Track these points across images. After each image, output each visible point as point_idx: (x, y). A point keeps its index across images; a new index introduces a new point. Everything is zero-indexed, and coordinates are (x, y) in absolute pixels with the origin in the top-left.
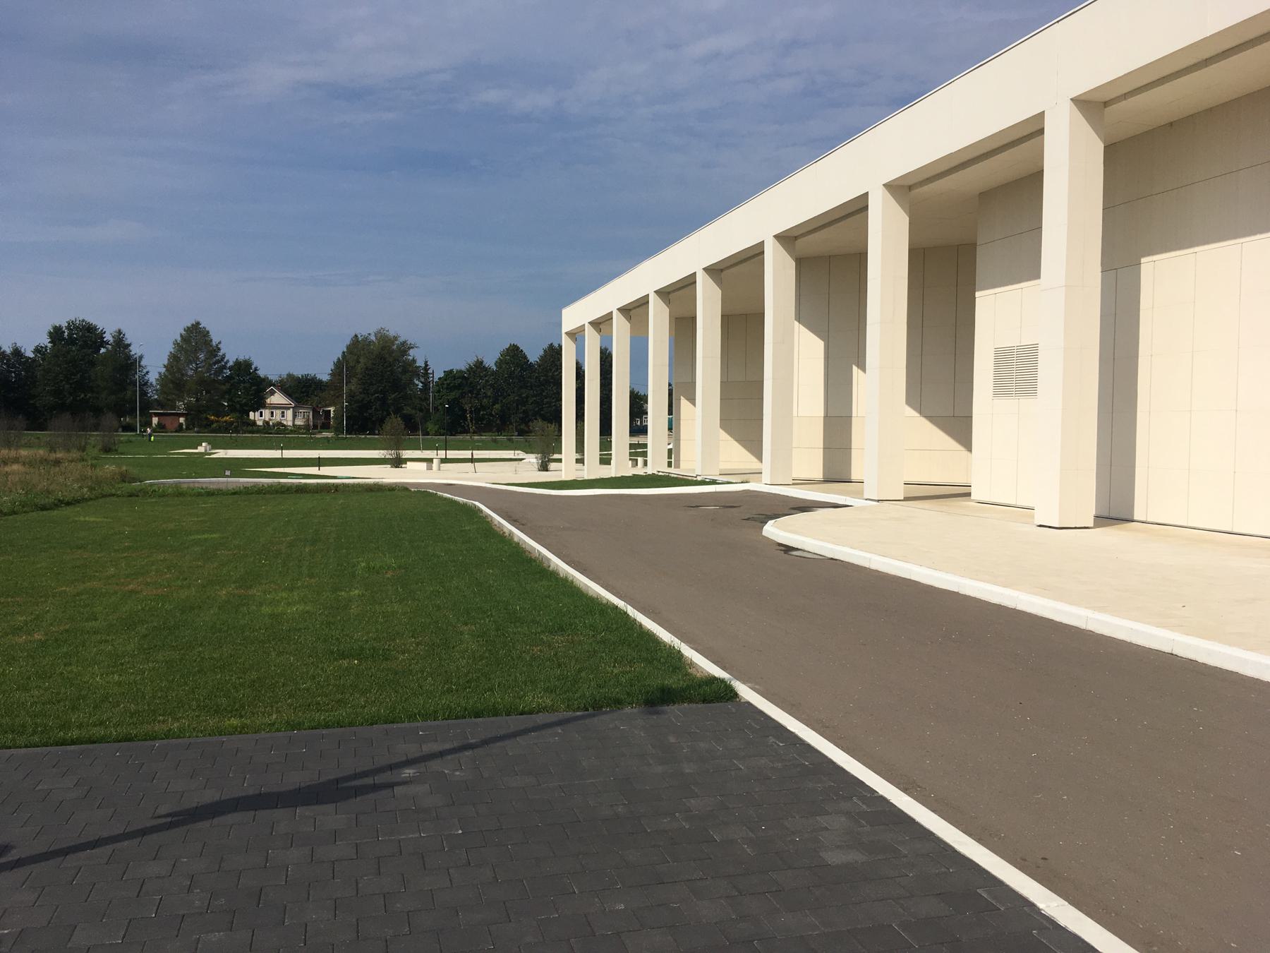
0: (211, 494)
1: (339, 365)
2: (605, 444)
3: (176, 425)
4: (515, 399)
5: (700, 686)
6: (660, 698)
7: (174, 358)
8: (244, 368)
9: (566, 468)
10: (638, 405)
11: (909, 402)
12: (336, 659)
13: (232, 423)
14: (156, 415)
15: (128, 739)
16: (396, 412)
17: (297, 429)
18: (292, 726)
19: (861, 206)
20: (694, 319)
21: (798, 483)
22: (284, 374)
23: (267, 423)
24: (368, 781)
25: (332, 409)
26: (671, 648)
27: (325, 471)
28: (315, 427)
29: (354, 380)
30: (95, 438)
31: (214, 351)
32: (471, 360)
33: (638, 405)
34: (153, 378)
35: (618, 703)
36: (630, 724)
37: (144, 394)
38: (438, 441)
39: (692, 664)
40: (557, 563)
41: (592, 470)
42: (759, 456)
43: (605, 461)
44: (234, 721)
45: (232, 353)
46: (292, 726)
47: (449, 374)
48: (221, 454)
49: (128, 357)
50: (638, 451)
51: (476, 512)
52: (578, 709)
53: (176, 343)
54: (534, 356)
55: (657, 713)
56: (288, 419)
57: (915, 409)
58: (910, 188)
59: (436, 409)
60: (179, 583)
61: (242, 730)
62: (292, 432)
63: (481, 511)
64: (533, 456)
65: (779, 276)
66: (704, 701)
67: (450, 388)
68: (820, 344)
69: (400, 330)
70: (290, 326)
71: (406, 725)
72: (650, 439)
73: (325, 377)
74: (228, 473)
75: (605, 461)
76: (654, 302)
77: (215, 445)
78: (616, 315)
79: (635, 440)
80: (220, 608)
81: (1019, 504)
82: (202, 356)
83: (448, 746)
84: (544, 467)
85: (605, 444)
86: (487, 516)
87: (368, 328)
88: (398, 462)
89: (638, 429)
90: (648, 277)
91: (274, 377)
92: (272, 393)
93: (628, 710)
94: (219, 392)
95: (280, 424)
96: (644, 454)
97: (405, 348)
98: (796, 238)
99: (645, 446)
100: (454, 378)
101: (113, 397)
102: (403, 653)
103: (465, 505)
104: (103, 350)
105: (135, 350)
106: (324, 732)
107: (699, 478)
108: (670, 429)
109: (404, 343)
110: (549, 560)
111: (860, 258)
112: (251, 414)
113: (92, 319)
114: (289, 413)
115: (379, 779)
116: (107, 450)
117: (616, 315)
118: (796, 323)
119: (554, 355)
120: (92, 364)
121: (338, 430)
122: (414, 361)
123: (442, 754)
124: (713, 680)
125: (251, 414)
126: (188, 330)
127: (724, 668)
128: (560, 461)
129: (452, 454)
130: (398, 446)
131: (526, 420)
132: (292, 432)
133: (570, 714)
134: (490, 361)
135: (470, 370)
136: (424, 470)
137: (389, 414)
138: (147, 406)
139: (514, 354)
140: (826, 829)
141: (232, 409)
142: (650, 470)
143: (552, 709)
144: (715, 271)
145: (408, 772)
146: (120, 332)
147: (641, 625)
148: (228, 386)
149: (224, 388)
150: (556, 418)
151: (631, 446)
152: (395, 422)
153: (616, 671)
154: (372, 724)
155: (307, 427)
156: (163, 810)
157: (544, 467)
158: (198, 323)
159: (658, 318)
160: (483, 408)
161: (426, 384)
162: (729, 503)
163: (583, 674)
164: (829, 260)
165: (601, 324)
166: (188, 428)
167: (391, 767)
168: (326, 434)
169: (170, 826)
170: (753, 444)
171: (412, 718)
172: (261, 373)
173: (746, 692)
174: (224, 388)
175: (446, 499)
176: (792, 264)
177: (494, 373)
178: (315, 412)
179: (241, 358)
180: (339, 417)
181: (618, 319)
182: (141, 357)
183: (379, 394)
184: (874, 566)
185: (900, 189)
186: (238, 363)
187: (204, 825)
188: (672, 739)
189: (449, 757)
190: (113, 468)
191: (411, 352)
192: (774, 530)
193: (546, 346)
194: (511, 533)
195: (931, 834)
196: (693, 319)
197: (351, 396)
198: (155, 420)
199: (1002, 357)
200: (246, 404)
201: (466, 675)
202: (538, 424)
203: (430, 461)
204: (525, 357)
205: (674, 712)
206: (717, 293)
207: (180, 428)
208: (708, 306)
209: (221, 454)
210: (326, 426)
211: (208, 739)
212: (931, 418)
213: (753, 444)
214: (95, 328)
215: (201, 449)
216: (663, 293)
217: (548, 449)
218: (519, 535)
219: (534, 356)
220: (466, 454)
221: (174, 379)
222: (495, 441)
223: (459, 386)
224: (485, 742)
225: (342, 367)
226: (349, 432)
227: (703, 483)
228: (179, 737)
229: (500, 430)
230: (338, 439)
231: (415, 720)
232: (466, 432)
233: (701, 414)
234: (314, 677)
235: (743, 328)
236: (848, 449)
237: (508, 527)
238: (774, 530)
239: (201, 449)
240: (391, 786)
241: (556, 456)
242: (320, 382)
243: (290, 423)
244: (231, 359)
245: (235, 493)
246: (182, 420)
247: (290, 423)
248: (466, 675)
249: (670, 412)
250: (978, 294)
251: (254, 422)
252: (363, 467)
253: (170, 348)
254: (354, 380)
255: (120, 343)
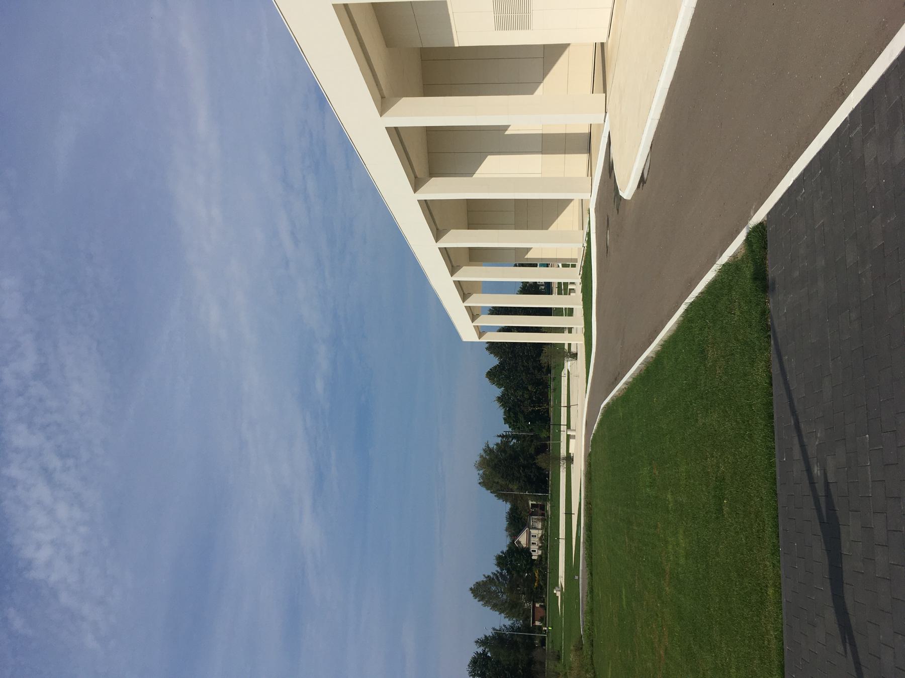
0: (591, 590)
1: (500, 496)
2: (558, 312)
3: (542, 610)
4: (525, 376)
5: (753, 251)
6: (761, 279)
7: (495, 607)
8: (501, 561)
9: (576, 341)
10: (530, 289)
11: (531, 92)
12: (723, 515)
13: (540, 571)
14: (534, 622)
15: (782, 667)
16: (534, 459)
17: (544, 528)
18: (775, 552)
19: (395, 132)
20: (470, 248)
21: (590, 172)
22: (506, 533)
23: (540, 548)
24: (822, 500)
25: (530, 503)
26: (720, 271)
27: (575, 510)
28: (543, 515)
29: (511, 486)
30: (550, 665)
31: (490, 580)
32: (497, 405)
33: (530, 289)
34: (508, 622)
35: (764, 313)
36: (781, 306)
37: (519, 629)
38: (554, 431)
39: (734, 256)
40: (650, 351)
41: (577, 321)
42: (569, 201)
43: (570, 312)
44: (771, 591)
45: (492, 568)
46: (775, 552)
47: (506, 421)
48: (562, 580)
49: (493, 637)
50: (564, 289)
51: (609, 409)
52: (769, 343)
53: (485, 605)
54: (494, 361)
55: (774, 284)
56: (537, 533)
57: (538, 87)
58: (383, 97)
59: (531, 430)
60: (660, 619)
61: (778, 588)
62: (546, 531)
63: (608, 404)
64: (566, 364)
65: (442, 189)
66: (765, 248)
67: (517, 420)
68: (490, 158)
69: (475, 453)
70: (472, 527)
71: (777, 469)
72: (554, 280)
73: (508, 506)
74: (576, 577)
75: (570, 312)
76: (458, 277)
77: (556, 584)
78: (468, 303)
79: (555, 290)
80: (680, 593)
81: (611, 5)
82: (493, 588)
83: (796, 440)
84: (575, 356)
85: (558, 312)
86: (612, 399)
87: (475, 475)
88: (569, 459)
89: (547, 289)
90: (442, 282)
91: (508, 541)
92: (519, 542)
93: (770, 306)
94: (518, 578)
95: (541, 539)
96: (566, 284)
97: (488, 450)
98: (416, 177)
99: (559, 284)
100: (509, 417)
101: (521, 650)
102: (719, 467)
103: (604, 415)
104: (489, 654)
105: (489, 633)
106: (781, 528)
107: (585, 245)
108: (547, 265)
109: (485, 451)
110: (647, 357)
111: (430, 131)
112: (533, 558)
113: (468, 659)
114: (533, 532)
115: (821, 492)
116: (558, 658)
117: (468, 303)
118: (475, 176)
119: (494, 347)
120: (498, 662)
121: (545, 499)
122: (497, 444)
123: (803, 446)
124: (748, 240)
125: (533, 558)
126: (475, 596)
127: (738, 232)
128: (570, 345)
129: (564, 421)
130: (558, 458)
131: (540, 368)
132: (546, 531)
133: (772, 348)
134: (498, 391)
135: (504, 406)
136: (575, 440)
137: (535, 464)
138: (527, 628)
139: (493, 375)
140: (876, 159)
141: (530, 570)
142: (578, 280)
143: (768, 361)
144: (438, 235)
145: (816, 470)
146: (477, 642)
147: (701, 293)
148: (514, 572)
149: (515, 575)
150: (539, 347)
151: (559, 293)
152: (540, 460)
153: (738, 313)
154: (776, 494)
155: (543, 520)
156: (840, 648)
157: (575, 356)
158: (471, 589)
159: (470, 274)
160: (531, 398)
161: (514, 437)
162: (604, 223)
163: (740, 338)
164: (432, 153)
165: (473, 314)
166: (543, 602)
167: (812, 483)
168: (548, 507)
169: (853, 645)
170: (560, 205)
171: (772, 465)
172: (505, 549)
173: (759, 216)
174: (515, 575)
175: (598, 427)
176: (434, 180)
177: (506, 390)
178: (532, 514)
179: (495, 562)
180: (536, 498)
181: (470, 302)
182: (494, 629)
183: (521, 468)
184: (658, 117)
185: (384, 104)
186: (498, 564)
187: (853, 621)
188: (797, 274)
189: (805, 440)
190: (572, 656)
191: (491, 446)
192: (627, 191)
193: (487, 352)
194: (626, 383)
195: (883, 77)
196: (471, 249)
197: (521, 489)
198: (537, 623)
199: (502, 25)
200: (527, 561)
201: (738, 423)
202: (543, 359)
203: (569, 437)
204: (495, 367)
205: (773, 271)
206: (453, 232)
207: (544, 607)
208: (462, 239)
209: (562, 580)
210: (543, 508)
211: (784, 612)
212: (544, 75)
213: (560, 205)
214: (474, 658)
215: (559, 594)
216: (453, 270)
217: (562, 353)
218: (627, 378)
219: (494, 361)
220: (564, 411)
221: (509, 608)
222: (555, 390)
223: (516, 414)
224: (794, 412)
225: (502, 494)
226: (547, 492)
227: (589, 242)
228: (782, 632)
229: (547, 386)
230: (552, 500)
231: (774, 462)
232: (548, 411)
233: (538, 243)
234: (737, 533)
235: (476, 214)
236: (566, 136)
237: (621, 385)
238: (627, 191)
239: (559, 594)
240: (827, 484)
241: (566, 347)
242: (511, 509)
243: (540, 532)
244: (495, 569)
245: (591, 574)
246: (537, 605)
247: (540, 532)
248: (738, 423)
249: (535, 265)
250: (456, 45)
251: (539, 556)
252: (573, 483)
253: (488, 609)
254: (511, 486)
255: (484, 642)
